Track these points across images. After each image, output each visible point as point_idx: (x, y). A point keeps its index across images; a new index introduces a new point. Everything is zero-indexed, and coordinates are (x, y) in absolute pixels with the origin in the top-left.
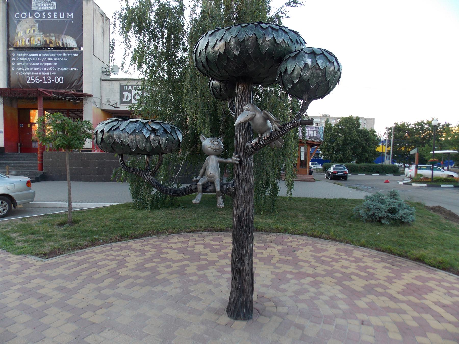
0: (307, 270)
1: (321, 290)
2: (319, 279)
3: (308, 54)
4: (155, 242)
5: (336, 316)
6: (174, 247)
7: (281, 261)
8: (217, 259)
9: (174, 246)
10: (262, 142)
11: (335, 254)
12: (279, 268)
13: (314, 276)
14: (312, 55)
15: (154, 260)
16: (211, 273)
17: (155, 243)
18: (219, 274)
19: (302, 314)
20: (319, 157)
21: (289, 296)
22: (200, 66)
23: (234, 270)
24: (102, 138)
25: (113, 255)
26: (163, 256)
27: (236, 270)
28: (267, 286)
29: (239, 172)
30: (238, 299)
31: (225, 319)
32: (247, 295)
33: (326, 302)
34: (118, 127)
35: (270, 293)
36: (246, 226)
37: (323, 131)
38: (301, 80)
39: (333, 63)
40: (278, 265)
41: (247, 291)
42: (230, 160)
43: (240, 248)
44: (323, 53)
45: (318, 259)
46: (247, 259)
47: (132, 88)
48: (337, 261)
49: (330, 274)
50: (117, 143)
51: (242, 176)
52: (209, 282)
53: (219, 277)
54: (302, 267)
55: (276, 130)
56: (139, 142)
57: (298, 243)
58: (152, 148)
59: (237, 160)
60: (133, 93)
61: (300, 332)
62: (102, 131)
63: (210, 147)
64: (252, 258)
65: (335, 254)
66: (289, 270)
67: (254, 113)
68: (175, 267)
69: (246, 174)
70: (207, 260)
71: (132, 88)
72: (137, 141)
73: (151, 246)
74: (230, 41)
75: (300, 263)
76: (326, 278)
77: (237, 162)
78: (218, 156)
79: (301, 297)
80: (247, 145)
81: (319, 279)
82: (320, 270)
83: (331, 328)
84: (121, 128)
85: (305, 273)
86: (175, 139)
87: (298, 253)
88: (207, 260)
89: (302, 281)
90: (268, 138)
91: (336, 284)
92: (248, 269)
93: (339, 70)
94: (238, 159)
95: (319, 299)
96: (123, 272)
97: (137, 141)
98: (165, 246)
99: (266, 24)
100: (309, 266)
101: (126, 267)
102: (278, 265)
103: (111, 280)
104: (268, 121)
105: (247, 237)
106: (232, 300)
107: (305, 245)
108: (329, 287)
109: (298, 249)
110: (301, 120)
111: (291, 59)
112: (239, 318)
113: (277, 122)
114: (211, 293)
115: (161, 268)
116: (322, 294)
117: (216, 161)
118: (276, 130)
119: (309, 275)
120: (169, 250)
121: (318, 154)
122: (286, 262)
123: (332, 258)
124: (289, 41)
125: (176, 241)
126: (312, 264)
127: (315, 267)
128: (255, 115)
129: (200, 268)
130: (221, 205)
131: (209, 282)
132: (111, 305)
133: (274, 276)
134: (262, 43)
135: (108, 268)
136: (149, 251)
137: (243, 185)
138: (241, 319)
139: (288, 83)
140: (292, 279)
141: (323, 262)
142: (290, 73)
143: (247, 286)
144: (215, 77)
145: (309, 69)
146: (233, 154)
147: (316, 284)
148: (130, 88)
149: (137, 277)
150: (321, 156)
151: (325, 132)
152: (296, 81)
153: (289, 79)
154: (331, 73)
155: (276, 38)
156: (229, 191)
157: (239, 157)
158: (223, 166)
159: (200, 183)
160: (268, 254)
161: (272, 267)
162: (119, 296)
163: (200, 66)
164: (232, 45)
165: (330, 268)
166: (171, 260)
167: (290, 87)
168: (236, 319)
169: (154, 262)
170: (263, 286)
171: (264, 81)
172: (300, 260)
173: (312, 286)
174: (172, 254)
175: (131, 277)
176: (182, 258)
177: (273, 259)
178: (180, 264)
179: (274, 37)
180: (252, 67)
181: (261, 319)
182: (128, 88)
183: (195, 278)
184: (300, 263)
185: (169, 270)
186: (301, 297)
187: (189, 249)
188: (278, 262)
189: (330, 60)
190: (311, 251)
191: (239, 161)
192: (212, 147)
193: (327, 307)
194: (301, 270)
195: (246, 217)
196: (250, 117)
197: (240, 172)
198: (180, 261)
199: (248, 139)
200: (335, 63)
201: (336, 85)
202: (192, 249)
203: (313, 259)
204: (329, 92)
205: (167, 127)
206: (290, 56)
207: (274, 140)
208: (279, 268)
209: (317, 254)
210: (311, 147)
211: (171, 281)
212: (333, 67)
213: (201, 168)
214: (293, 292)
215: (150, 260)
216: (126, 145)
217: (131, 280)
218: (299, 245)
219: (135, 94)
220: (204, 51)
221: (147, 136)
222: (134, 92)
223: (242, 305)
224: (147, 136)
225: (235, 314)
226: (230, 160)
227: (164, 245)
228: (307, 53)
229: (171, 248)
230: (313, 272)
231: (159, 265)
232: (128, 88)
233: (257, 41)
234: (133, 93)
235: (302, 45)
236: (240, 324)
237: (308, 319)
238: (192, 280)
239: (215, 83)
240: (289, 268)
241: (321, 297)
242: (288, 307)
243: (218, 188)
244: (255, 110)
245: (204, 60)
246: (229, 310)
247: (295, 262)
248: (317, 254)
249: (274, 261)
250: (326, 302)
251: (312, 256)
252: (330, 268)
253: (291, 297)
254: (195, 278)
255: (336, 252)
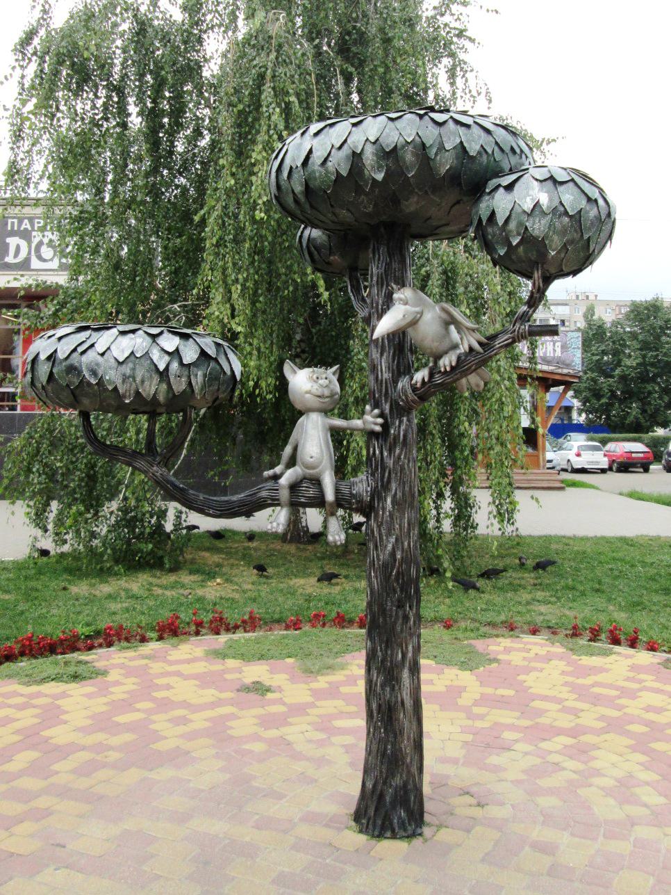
0: (555, 720)
1: (597, 764)
2: (588, 738)
3: (541, 181)
4: (131, 659)
5: (632, 822)
6: (186, 673)
7: (484, 700)
8: (310, 699)
9: (186, 669)
10: (438, 379)
11: (628, 679)
12: (481, 717)
13: (574, 732)
14: (549, 183)
15: (139, 706)
16: (298, 732)
17: (132, 664)
18: (322, 736)
19: (548, 819)
20: (570, 418)
21: (512, 781)
22: (290, 200)
23: (374, 706)
24: (51, 374)
25: (22, 695)
26: (159, 695)
27: (380, 706)
28: (455, 761)
29: (381, 453)
30: (385, 783)
31: (355, 839)
32: (409, 772)
33: (608, 792)
34: (92, 345)
35: (464, 775)
36: (402, 591)
37: (580, 344)
38: (527, 239)
39: (596, 201)
40: (476, 710)
41: (408, 760)
42: (357, 423)
43: (387, 647)
44: (572, 180)
45: (582, 693)
46: (406, 674)
47: (32, 225)
48: (632, 695)
49: (613, 726)
50: (89, 384)
51: (390, 463)
52: (297, 757)
53: (321, 743)
54: (541, 713)
55: (471, 349)
56: (143, 382)
57: (525, 655)
58: (171, 395)
59: (376, 424)
60: (35, 242)
61: (547, 861)
62: (52, 357)
63: (307, 392)
64: (419, 673)
65: (628, 679)
66: (509, 721)
67: (417, 309)
68: (199, 721)
69: (399, 458)
70: (284, 704)
71: (32, 225)
72: (138, 379)
73: (123, 671)
74: (363, 149)
75: (537, 704)
76: (607, 737)
77: (378, 428)
78: (326, 412)
79: (545, 782)
80: (400, 385)
81: (588, 738)
82: (590, 717)
83: (622, 847)
84: (100, 348)
85: (552, 727)
86: (225, 373)
87: (529, 679)
88: (284, 704)
89: (544, 745)
90: (452, 368)
91: (634, 749)
92: (408, 703)
93: (609, 215)
94: (380, 420)
95: (590, 785)
96: (59, 735)
97: (138, 379)
98: (162, 671)
99: (441, 112)
100: (559, 711)
101: (65, 722)
102: (476, 710)
103: (32, 755)
104: (452, 328)
105: (406, 618)
106: (369, 785)
107: (548, 658)
108: (615, 758)
109: (527, 670)
110: (530, 326)
111: (501, 190)
112: (388, 834)
113: (473, 330)
114: (305, 779)
115: (160, 723)
116: (598, 773)
117: (324, 425)
118: (471, 349)
119: (560, 732)
120: (172, 680)
121: (568, 409)
122: (502, 702)
123: (617, 688)
124: (496, 149)
125: (190, 656)
126: (567, 704)
127: (575, 712)
128: (422, 313)
129: (268, 722)
130: (337, 538)
131: (297, 757)
132: (47, 813)
133: (470, 737)
134: (436, 154)
135: (17, 725)
136: (117, 683)
137: (394, 486)
138: (394, 836)
139: (497, 243)
140: (516, 741)
141: (597, 700)
142: (500, 222)
143: (406, 746)
144: (320, 224)
145: (544, 214)
146: (368, 407)
147: (581, 752)
148: (26, 225)
149: (100, 748)
150: (580, 415)
151: (586, 344)
152: (515, 242)
153: (501, 234)
154: (592, 223)
155: (465, 145)
156: (358, 502)
157: (381, 415)
158: (338, 438)
159: (283, 481)
160: (448, 683)
161: (463, 715)
162: (65, 793)
163: (290, 200)
164: (367, 159)
165: (615, 714)
166: (185, 704)
167: (502, 252)
168: (380, 836)
169: (138, 710)
170: (444, 760)
171: (437, 231)
172: (534, 697)
173: (571, 757)
174: (184, 690)
175: (84, 748)
176: (212, 699)
177: (464, 695)
178: (210, 713)
179: (461, 142)
180: (411, 205)
181: (444, 835)
182: (19, 226)
183: (258, 747)
184: (537, 704)
185: (181, 729)
186: (545, 782)
187: (228, 676)
188: (476, 703)
189: (590, 195)
190: (563, 673)
191: (382, 425)
192: (314, 391)
193: (612, 801)
194: (542, 720)
195: (401, 565)
196: (409, 319)
197: (385, 454)
198: (213, 705)
199: (403, 369)
200: (601, 202)
201: (604, 246)
202: (237, 676)
203: (569, 692)
204: (591, 263)
205: (207, 345)
206: (499, 185)
207: (465, 373)
208: (481, 717)
209: (580, 681)
210: (547, 389)
211: (193, 754)
212: (596, 209)
213: (285, 442)
214: (523, 772)
215: (126, 705)
216: (110, 388)
217: (84, 756)
218: (530, 660)
219: (40, 243)
220: (300, 168)
221: (162, 367)
222: (37, 237)
223: (392, 801)
224: (162, 367)
225: (379, 822)
226: (357, 423)
227: (156, 667)
228: (537, 180)
229: (178, 674)
230: (573, 724)
231: (154, 717)
232: (19, 226)
233: (424, 149)
234: (35, 242)
235: (524, 156)
236: (388, 846)
237: (564, 829)
238: (251, 752)
239: (316, 233)
240: (506, 717)
241: (597, 781)
242: (513, 806)
243: (330, 496)
244: (419, 302)
245: (298, 188)
246: (358, 817)
247: (523, 702)
248: (580, 681)
249: (465, 700)
250: (608, 792)
251: (566, 684)
252: (615, 714)
253: (517, 782)
254: (258, 747)
255: (631, 674)
